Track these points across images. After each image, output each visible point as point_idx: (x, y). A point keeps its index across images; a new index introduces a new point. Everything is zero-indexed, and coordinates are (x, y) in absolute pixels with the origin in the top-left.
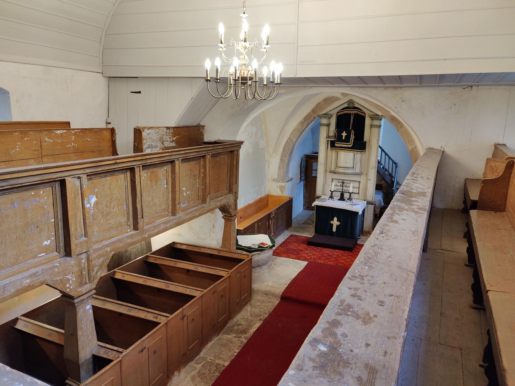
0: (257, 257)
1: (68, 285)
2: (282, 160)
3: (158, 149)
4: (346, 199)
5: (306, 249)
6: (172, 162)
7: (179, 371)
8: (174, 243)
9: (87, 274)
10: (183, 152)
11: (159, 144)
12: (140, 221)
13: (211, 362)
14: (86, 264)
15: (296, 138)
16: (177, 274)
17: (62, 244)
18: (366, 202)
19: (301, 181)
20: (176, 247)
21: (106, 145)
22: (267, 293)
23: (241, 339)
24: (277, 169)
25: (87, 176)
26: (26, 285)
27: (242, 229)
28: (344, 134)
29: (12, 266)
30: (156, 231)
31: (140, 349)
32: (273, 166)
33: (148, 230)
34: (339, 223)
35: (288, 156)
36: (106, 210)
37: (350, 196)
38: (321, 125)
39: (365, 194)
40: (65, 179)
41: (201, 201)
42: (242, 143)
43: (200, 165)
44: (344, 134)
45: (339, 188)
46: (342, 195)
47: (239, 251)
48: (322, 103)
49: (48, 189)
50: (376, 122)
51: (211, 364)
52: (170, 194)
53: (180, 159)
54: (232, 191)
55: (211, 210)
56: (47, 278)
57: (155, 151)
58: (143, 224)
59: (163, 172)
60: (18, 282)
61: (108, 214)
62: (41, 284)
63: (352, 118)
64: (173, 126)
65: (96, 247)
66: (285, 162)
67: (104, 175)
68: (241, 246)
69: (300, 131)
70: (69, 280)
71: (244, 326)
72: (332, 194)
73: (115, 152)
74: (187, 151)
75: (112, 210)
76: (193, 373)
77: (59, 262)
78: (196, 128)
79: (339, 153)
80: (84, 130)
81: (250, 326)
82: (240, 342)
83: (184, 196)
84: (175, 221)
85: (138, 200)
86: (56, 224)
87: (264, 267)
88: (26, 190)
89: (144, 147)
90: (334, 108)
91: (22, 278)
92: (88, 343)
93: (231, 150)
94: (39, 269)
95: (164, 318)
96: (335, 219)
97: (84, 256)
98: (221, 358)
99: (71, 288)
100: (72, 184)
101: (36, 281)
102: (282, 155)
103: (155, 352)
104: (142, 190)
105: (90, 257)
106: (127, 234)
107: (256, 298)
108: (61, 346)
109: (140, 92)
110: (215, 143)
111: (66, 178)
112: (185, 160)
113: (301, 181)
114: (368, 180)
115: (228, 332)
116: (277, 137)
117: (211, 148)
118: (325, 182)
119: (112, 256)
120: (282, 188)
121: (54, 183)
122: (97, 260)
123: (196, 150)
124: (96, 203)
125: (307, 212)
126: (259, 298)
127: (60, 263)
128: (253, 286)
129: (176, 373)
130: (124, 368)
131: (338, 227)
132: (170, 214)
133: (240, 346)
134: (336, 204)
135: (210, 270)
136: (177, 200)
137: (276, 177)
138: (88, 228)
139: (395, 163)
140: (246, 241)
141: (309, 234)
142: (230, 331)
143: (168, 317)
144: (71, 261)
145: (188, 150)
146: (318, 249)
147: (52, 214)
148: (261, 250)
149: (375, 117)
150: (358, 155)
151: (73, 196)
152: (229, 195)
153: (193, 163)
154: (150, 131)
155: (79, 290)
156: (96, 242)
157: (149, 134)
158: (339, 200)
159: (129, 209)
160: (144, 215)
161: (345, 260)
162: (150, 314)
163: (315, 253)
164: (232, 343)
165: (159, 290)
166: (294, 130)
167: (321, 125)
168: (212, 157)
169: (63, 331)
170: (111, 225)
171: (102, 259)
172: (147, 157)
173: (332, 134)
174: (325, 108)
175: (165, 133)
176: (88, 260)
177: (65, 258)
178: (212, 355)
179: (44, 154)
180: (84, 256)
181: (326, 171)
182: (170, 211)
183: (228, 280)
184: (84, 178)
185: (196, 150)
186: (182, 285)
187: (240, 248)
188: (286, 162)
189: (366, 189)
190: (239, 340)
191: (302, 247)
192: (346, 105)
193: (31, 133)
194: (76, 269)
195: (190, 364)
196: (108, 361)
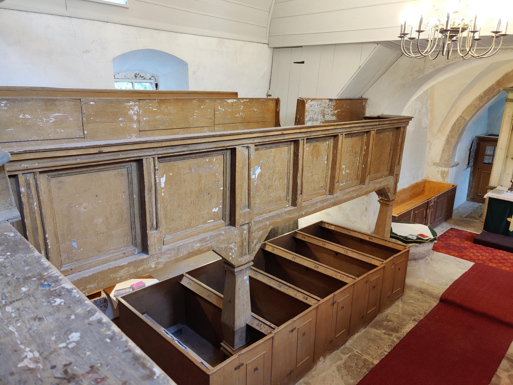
0: (415, 249)
1: (230, 254)
2: (448, 142)
3: (319, 122)
6: (335, 136)
7: (325, 357)
8: (322, 222)
10: (348, 126)
11: (320, 118)
12: (299, 197)
13: (358, 356)
15: (470, 116)
16: (325, 255)
17: (228, 213)
21: (270, 116)
22: (422, 291)
23: (391, 338)
25: (255, 146)
26: (197, 249)
27: (397, 216)
29: (186, 229)
30: (313, 209)
31: (290, 328)
32: (436, 147)
33: (306, 207)
35: (456, 137)
40: (235, 148)
41: (359, 181)
42: (410, 118)
47: (393, 240)
49: (220, 156)
51: (358, 357)
52: (330, 171)
53: (344, 133)
54: (393, 173)
55: (367, 193)
56: (213, 244)
57: (315, 124)
58: (301, 200)
59: (325, 146)
60: (190, 245)
61: (269, 187)
62: (208, 250)
64: (336, 98)
65: (257, 219)
67: (270, 146)
68: (396, 234)
69: (475, 108)
70: (231, 249)
71: (395, 323)
73: (277, 123)
74: (352, 125)
75: (274, 183)
76: (339, 363)
77: (225, 230)
78: (359, 101)
80: (251, 100)
81: (402, 326)
82: (391, 341)
83: (342, 174)
86: (224, 194)
87: (421, 261)
88: (202, 157)
91: (194, 242)
92: (243, 315)
93: (397, 127)
94: (207, 235)
95: (314, 301)
97: (246, 227)
98: (369, 354)
99: (233, 257)
100: (241, 153)
101: (205, 246)
102: (448, 136)
103: (304, 334)
104: (304, 164)
106: (286, 210)
107: (408, 293)
108: (220, 310)
109: (303, 62)
110: (378, 118)
111: (237, 147)
112: (349, 135)
113: (468, 167)
115: (377, 326)
117: (378, 123)
118: (504, 170)
119: (270, 232)
120: (444, 174)
121: (226, 151)
122: (257, 232)
123: (361, 125)
124: (260, 175)
125: (471, 204)
126: (412, 294)
127: (225, 232)
128: (406, 280)
129: (321, 359)
130: (275, 344)
132: (327, 193)
133: (391, 346)
135: (361, 256)
136: (336, 178)
137: (438, 160)
140: (403, 229)
142: (378, 326)
143: (319, 301)
144: (234, 231)
146: (488, 249)
147: (221, 183)
148: (420, 243)
151: (241, 165)
152: (389, 177)
153: (355, 139)
154: (313, 102)
156: (257, 214)
157: (311, 106)
162: (300, 294)
163: (485, 254)
164: (381, 339)
165: (307, 269)
166: (469, 107)
168: (377, 133)
169: (222, 296)
170: (271, 199)
171: (261, 232)
172: (313, 129)
175: (327, 105)
177: (230, 227)
178: (359, 348)
179: (216, 122)
180: (246, 227)
182: (328, 189)
183: (382, 270)
184: (252, 147)
185: (361, 125)
186: (332, 268)
190: (390, 339)
191: (466, 244)
193: (207, 101)
194: (238, 239)
195: (335, 352)
196: (262, 335)
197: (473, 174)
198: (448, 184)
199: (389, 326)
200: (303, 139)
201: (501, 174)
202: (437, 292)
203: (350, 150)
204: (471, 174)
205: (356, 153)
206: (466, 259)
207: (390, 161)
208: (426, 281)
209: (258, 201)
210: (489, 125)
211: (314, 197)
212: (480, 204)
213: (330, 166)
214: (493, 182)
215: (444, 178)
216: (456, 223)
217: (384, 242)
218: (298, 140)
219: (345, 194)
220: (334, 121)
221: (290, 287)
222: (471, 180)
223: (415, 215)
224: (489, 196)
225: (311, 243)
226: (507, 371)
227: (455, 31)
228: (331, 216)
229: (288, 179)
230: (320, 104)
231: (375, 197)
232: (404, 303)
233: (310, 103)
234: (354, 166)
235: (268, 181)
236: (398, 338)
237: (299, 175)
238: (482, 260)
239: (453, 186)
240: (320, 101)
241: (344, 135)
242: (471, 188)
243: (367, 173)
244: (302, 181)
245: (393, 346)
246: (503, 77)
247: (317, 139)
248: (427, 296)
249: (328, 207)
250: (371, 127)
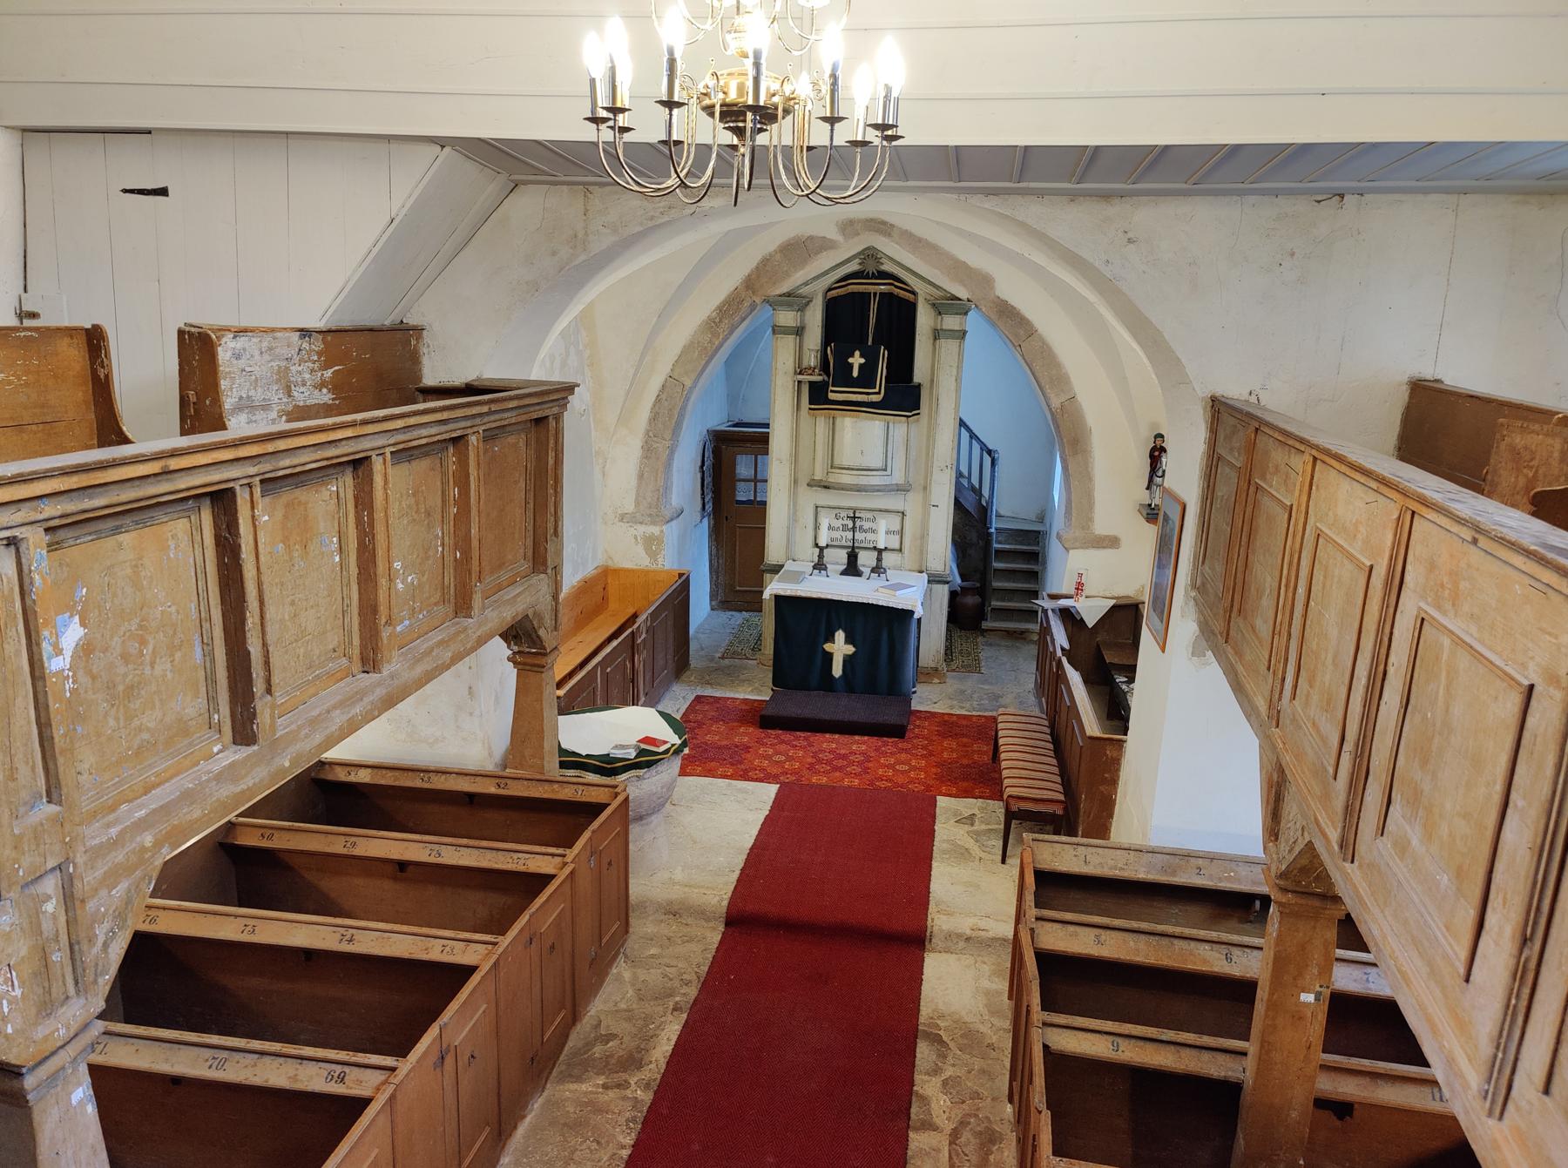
0: (639, 786)
2: (648, 451)
3: (274, 415)
4: (866, 571)
5: (760, 742)
6: (359, 464)
9: (67, 962)
10: (399, 424)
11: (276, 396)
12: (262, 705)
14: (62, 919)
15: (693, 376)
16: (360, 881)
18: (925, 576)
20: (330, 777)
21: (72, 399)
23: (628, 1093)
24: (634, 482)
25: (47, 530)
28: (857, 360)
34: (850, 649)
35: (668, 435)
36: (125, 675)
37: (879, 559)
38: (777, 330)
39: (922, 552)
41: (450, 609)
43: (444, 474)
44: (857, 360)
45: (837, 534)
46: (853, 557)
48: (778, 257)
50: (951, 322)
52: (355, 587)
54: (545, 563)
59: (327, 503)
63: (874, 307)
64: (320, 325)
65: (95, 834)
66: (655, 455)
67: (110, 523)
72: (821, 556)
73: (109, 431)
74: (412, 421)
75: (148, 671)
78: (399, 335)
79: (838, 421)
82: (628, 1106)
83: (397, 590)
84: (380, 692)
85: (249, 622)
87: (655, 819)
89: (228, 403)
95: (377, 1077)
96: (840, 636)
97: (50, 885)
102: (647, 432)
104: (264, 578)
105: (78, 884)
107: (642, 927)
109: (163, 192)
110: (469, 390)
112: (405, 454)
114: (928, 506)
115: (576, 1072)
116: (632, 371)
117: (485, 409)
118: (794, 518)
120: (651, 544)
122: (103, 893)
123: (438, 416)
124: (85, 650)
125: (724, 616)
126: (650, 929)
131: (848, 660)
132: (357, 667)
133: (634, 1120)
134: (835, 587)
135: (489, 854)
136: (383, 609)
137: (629, 507)
138: (61, 760)
139: (990, 452)
141: (756, 689)
142: (582, 1067)
143: (393, 1069)
145: (415, 413)
146: (797, 738)
148: (649, 765)
149: (948, 304)
150: (899, 427)
152: (535, 579)
154: (241, 342)
155: (40, 1032)
156: (94, 815)
157: (238, 357)
158: (844, 573)
159: (213, 661)
160: (275, 680)
161: (892, 766)
162: (312, 1068)
163: (794, 751)
165: (309, 956)
166: (686, 350)
167: (777, 330)
168: (486, 440)
170: (145, 736)
172: (282, 445)
173: (812, 360)
174: (787, 275)
175: (294, 352)
176: (69, 898)
182: (357, 652)
184: (35, 539)
185: (438, 416)
186: (405, 928)
187: (571, 761)
188: (664, 457)
189: (923, 536)
190: (624, 1098)
191: (746, 734)
192: (854, 267)
194: (21, 948)
197: (716, 533)
198: (668, 572)
199: (611, 1056)
200: (250, 485)
202: (715, 901)
203: (409, 507)
205: (428, 514)
206: (756, 780)
207: (531, 528)
208: (679, 875)
209: (87, 758)
210: (733, 398)
211: (312, 691)
213: (354, 570)
214: (774, 550)
215: (653, 555)
216: (708, 677)
217: (547, 786)
218: (231, 491)
219: (418, 661)
220: (327, 410)
221: (262, 1053)
223: (607, 678)
225: (302, 852)
226: (936, 1071)
227: (766, 115)
228: (371, 745)
229: (207, 645)
230: (270, 349)
231: (499, 649)
232: (633, 962)
233: (232, 344)
234: (427, 558)
235: (122, 670)
236: (647, 1086)
237: (252, 621)
238: (795, 772)
239: (681, 575)
240: (268, 338)
241: (388, 456)
243: (474, 576)
244: (265, 645)
245: (640, 1116)
247: (297, 478)
248: (690, 921)
249: (369, 717)
250: (469, 423)
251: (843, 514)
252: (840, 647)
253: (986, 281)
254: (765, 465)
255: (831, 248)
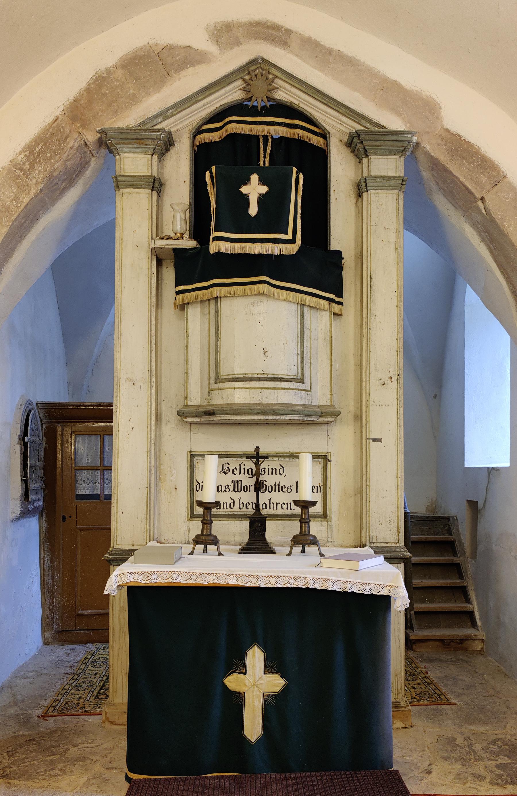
19: (25, 514)
28: (254, 189)
34: (276, 683)
38: (120, 182)
39: (360, 517)
44: (254, 189)
46: (257, 523)
48: (120, 74)
50: (385, 165)
79: (225, 305)
90: (183, 100)
96: (255, 657)
114: (363, 441)
118: (156, 474)
125: (60, 652)
131: (272, 705)
150: (320, 321)
158: (247, 549)
167: (120, 182)
174: (135, 100)
181: (158, 417)
189: (360, 490)
192: (233, 94)
197: (50, 541)
201: (149, 488)
204: (41, 544)
212: (91, 647)
222: (47, 564)
224: (127, 580)
242: (52, 592)
246: (88, 90)
251: (234, 464)
252: (256, 681)
253: (429, 108)
254: (111, 444)
255: (199, 62)
